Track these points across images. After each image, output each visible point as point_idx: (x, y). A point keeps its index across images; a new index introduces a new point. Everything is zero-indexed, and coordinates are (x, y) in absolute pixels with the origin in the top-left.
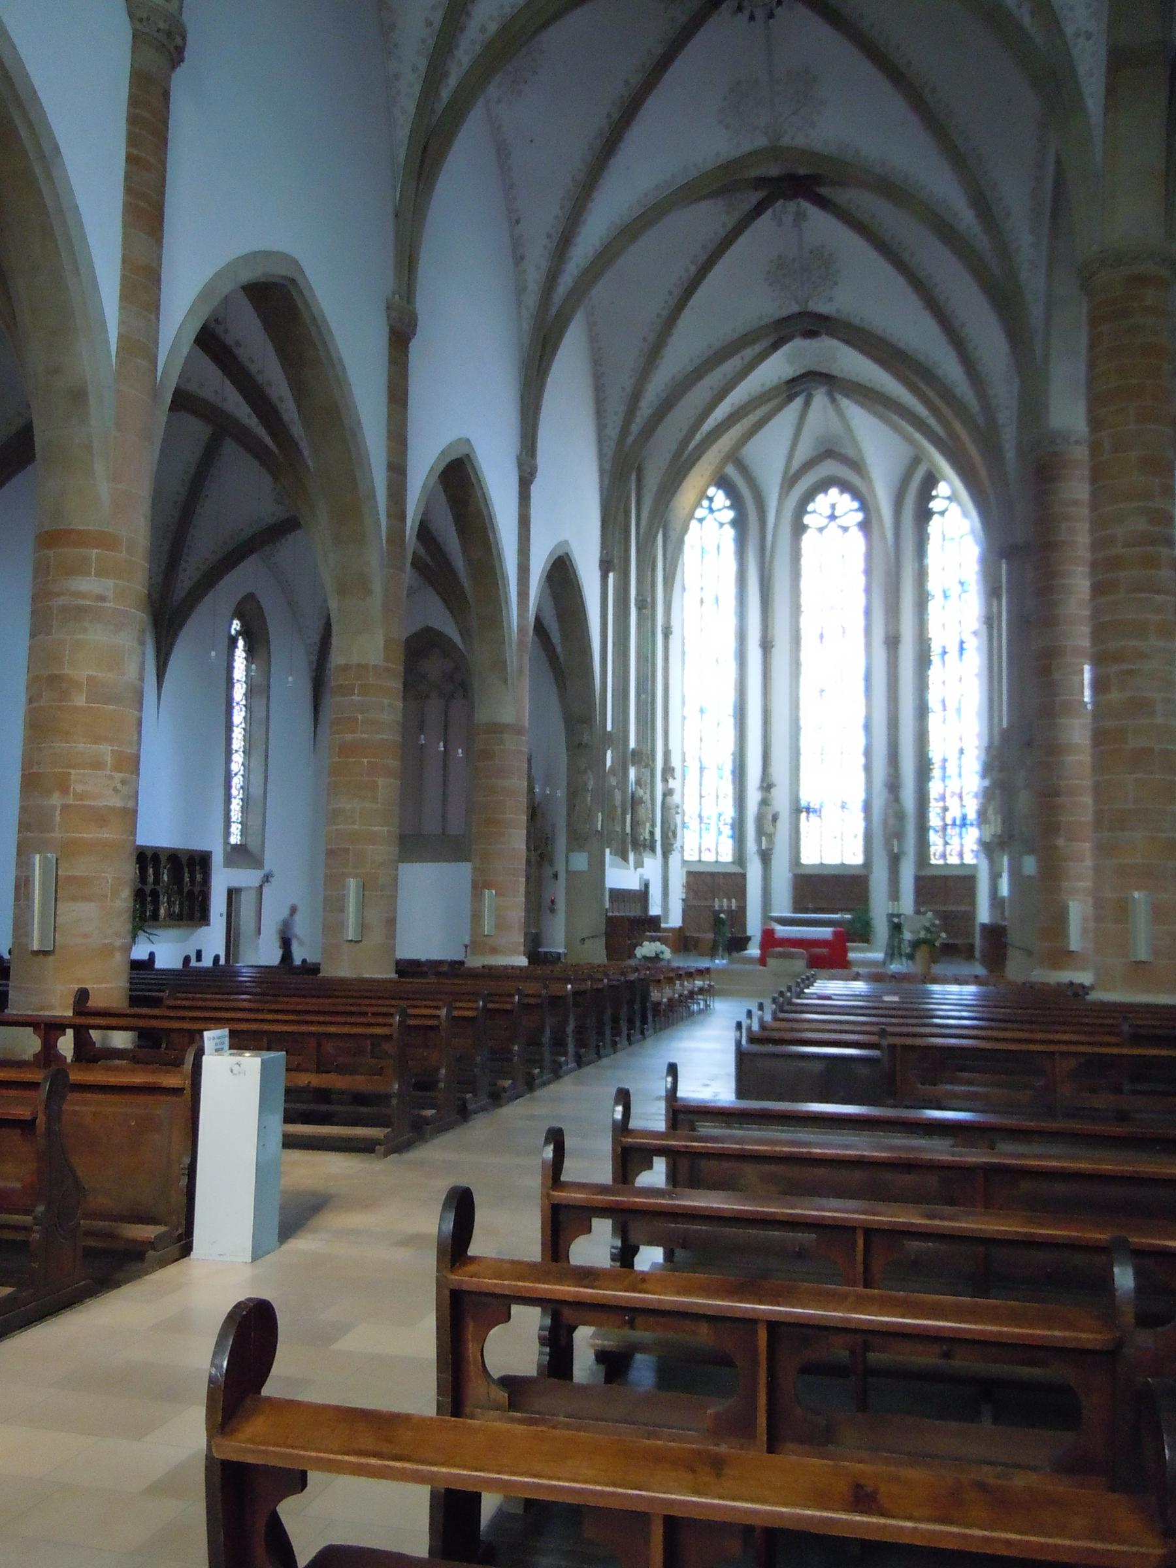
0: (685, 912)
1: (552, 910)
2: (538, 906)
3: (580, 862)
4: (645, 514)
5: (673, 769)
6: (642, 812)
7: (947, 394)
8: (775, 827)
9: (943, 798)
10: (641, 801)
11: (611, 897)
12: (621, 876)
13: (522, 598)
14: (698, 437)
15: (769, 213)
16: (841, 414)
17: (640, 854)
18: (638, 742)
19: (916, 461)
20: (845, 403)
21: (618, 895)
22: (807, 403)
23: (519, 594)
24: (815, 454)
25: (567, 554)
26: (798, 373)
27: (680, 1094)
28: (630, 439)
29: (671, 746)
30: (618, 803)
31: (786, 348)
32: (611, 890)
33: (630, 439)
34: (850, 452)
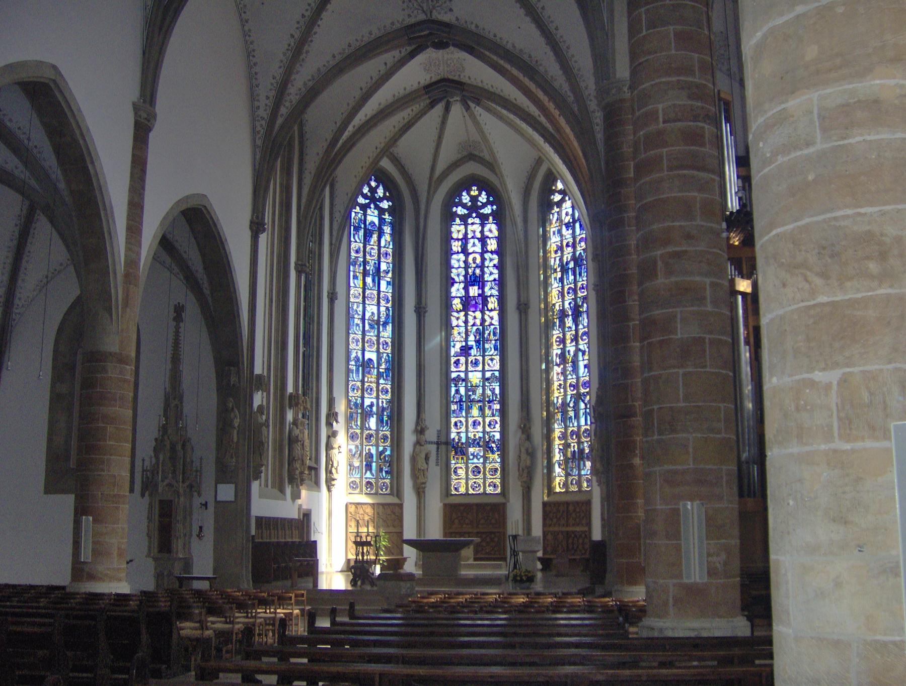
2: (165, 531)
5: (337, 414)
7: (546, 86)
13: (134, 234)
14: (350, 129)
15: (736, 472)
16: (473, 117)
17: (298, 487)
19: (539, 162)
20: (478, 110)
22: (447, 109)
23: (129, 229)
24: (460, 156)
26: (434, 80)
28: (280, 121)
31: (420, 58)
33: (280, 121)
34: (486, 156)
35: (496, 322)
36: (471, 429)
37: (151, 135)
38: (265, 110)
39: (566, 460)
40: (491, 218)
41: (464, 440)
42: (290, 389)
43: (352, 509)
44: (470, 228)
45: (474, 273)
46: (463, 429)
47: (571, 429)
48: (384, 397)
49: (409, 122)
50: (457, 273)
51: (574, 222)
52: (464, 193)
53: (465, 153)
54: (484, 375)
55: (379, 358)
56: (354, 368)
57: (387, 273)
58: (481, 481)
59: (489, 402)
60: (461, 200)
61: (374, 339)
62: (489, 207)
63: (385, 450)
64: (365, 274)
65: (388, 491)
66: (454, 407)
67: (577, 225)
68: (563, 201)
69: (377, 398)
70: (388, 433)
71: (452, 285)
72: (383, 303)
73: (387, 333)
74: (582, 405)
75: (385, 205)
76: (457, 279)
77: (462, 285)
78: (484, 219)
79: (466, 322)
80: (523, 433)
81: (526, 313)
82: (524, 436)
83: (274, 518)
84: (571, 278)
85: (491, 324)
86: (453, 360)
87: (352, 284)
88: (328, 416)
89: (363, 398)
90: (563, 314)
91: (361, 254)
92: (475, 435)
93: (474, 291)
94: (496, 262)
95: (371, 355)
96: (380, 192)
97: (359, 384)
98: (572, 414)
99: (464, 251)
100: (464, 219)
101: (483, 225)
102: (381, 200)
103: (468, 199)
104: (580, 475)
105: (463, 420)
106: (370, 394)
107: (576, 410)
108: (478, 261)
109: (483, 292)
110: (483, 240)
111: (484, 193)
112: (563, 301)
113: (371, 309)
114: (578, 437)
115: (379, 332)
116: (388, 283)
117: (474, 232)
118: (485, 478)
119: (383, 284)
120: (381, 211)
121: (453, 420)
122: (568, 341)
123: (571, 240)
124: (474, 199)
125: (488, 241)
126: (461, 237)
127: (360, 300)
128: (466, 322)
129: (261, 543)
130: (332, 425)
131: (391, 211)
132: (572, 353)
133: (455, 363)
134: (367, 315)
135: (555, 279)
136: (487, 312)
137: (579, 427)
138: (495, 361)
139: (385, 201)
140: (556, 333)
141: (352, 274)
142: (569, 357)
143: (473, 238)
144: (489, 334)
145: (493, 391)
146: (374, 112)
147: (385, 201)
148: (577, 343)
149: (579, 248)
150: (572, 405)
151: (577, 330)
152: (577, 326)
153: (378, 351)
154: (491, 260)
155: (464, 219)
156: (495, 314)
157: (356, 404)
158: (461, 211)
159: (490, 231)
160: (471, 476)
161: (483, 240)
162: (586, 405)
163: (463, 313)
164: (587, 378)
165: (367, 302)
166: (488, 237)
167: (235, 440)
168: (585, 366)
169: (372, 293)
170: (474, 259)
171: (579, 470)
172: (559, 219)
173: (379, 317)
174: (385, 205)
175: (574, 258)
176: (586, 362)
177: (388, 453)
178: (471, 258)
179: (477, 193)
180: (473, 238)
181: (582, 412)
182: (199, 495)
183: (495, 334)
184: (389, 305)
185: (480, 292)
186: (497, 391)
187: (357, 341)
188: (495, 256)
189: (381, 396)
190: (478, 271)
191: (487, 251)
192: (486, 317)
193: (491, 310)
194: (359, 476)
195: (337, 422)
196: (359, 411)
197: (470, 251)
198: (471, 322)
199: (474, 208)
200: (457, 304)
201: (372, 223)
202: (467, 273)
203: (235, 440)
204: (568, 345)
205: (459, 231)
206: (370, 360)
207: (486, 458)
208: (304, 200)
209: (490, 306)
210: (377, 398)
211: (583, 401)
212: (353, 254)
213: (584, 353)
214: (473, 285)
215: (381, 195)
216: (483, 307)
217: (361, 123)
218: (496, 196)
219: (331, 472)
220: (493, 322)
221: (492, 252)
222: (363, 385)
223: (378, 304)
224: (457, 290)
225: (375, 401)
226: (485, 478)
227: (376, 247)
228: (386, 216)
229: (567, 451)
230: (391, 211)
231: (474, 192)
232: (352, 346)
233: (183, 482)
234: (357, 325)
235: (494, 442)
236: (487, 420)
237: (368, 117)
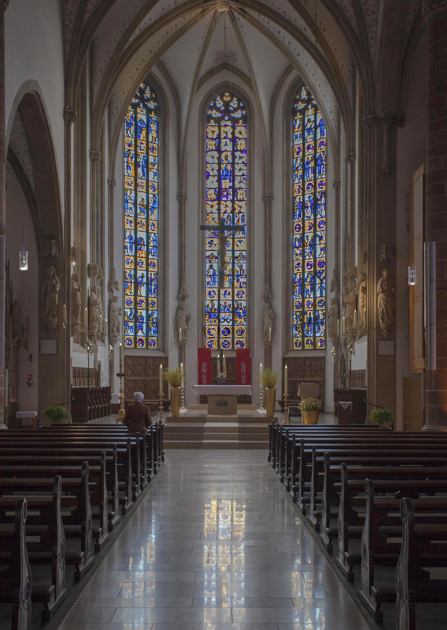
3: (50, 347)
10: (96, 303)
11: (74, 373)
12: (79, 358)
18: (92, 260)
21: (79, 372)
25: (37, 93)
28: (87, 16)
29: (115, 267)
30: (79, 302)
32: (75, 368)
33: (87, 16)
34: (241, 64)
35: (244, 210)
36: (222, 297)
37: (6, 14)
38: (74, 5)
39: (303, 325)
40: (241, 121)
41: (216, 307)
42: (88, 261)
43: (130, 362)
44: (223, 129)
45: (226, 169)
46: (216, 297)
47: (307, 300)
49: (181, 29)
50: (212, 168)
51: (316, 127)
53: (221, 62)
54: (233, 254)
55: (148, 238)
57: (154, 165)
58: (230, 340)
60: (215, 104)
61: (144, 221)
62: (239, 111)
63: (152, 314)
64: (137, 165)
67: (318, 130)
68: (306, 108)
69: (147, 270)
70: (155, 300)
71: (208, 177)
72: (151, 191)
74: (318, 281)
75: (152, 105)
76: (211, 173)
77: (216, 178)
78: (235, 121)
79: (219, 210)
81: (270, 204)
82: (267, 305)
84: (311, 175)
88: (110, 284)
89: (136, 270)
90: (303, 206)
91: (133, 148)
92: (225, 303)
94: (244, 160)
95: (142, 235)
96: (148, 94)
97: (132, 258)
98: (308, 287)
99: (218, 149)
100: (218, 121)
102: (148, 100)
103: (222, 103)
104: (315, 337)
106: (141, 267)
108: (230, 159)
109: (233, 184)
110: (234, 140)
111: (235, 99)
112: (303, 195)
113: (142, 195)
114: (314, 305)
115: (148, 215)
116: (155, 174)
117: (226, 133)
118: (233, 338)
119: (151, 174)
120: (149, 111)
121: (208, 290)
124: (226, 104)
125: (239, 142)
126: (215, 136)
127: (132, 187)
128: (219, 210)
129: (76, 388)
131: (157, 110)
132: (310, 239)
134: (139, 200)
136: (237, 202)
137: (315, 298)
138: (242, 243)
142: (308, 241)
144: (238, 221)
145: (241, 267)
147: (152, 102)
148: (315, 231)
149: (318, 151)
150: (308, 280)
151: (315, 220)
152: (315, 216)
153: (147, 232)
154: (241, 158)
155: (218, 121)
158: (215, 114)
159: (240, 133)
161: (234, 140)
162: (322, 281)
163: (217, 202)
165: (138, 190)
166: (238, 138)
167: (57, 302)
168: (322, 249)
170: (226, 157)
171: (315, 333)
173: (148, 203)
175: (315, 159)
176: (323, 246)
177: (155, 316)
179: (229, 99)
181: (317, 286)
182: (26, 348)
184: (156, 193)
185: (231, 184)
186: (244, 267)
187: (131, 222)
189: (150, 269)
190: (229, 167)
191: (237, 150)
192: (236, 206)
193: (240, 201)
195: (117, 289)
197: (223, 149)
198: (223, 209)
199: (227, 111)
201: (141, 121)
202: (220, 168)
203: (57, 302)
204: (306, 231)
205: (213, 132)
206: (141, 239)
207: (233, 321)
208: (95, 96)
209: (239, 197)
210: (147, 270)
211: (319, 277)
212: (127, 147)
214: (225, 179)
215: (149, 96)
216: (233, 198)
217: (146, 26)
220: (242, 210)
225: (145, 273)
226: (233, 338)
227: (144, 142)
228: (153, 115)
229: (303, 317)
230: (157, 110)
233: (13, 337)
234: (131, 208)
235: (241, 309)
236: (236, 291)
237: (153, 21)
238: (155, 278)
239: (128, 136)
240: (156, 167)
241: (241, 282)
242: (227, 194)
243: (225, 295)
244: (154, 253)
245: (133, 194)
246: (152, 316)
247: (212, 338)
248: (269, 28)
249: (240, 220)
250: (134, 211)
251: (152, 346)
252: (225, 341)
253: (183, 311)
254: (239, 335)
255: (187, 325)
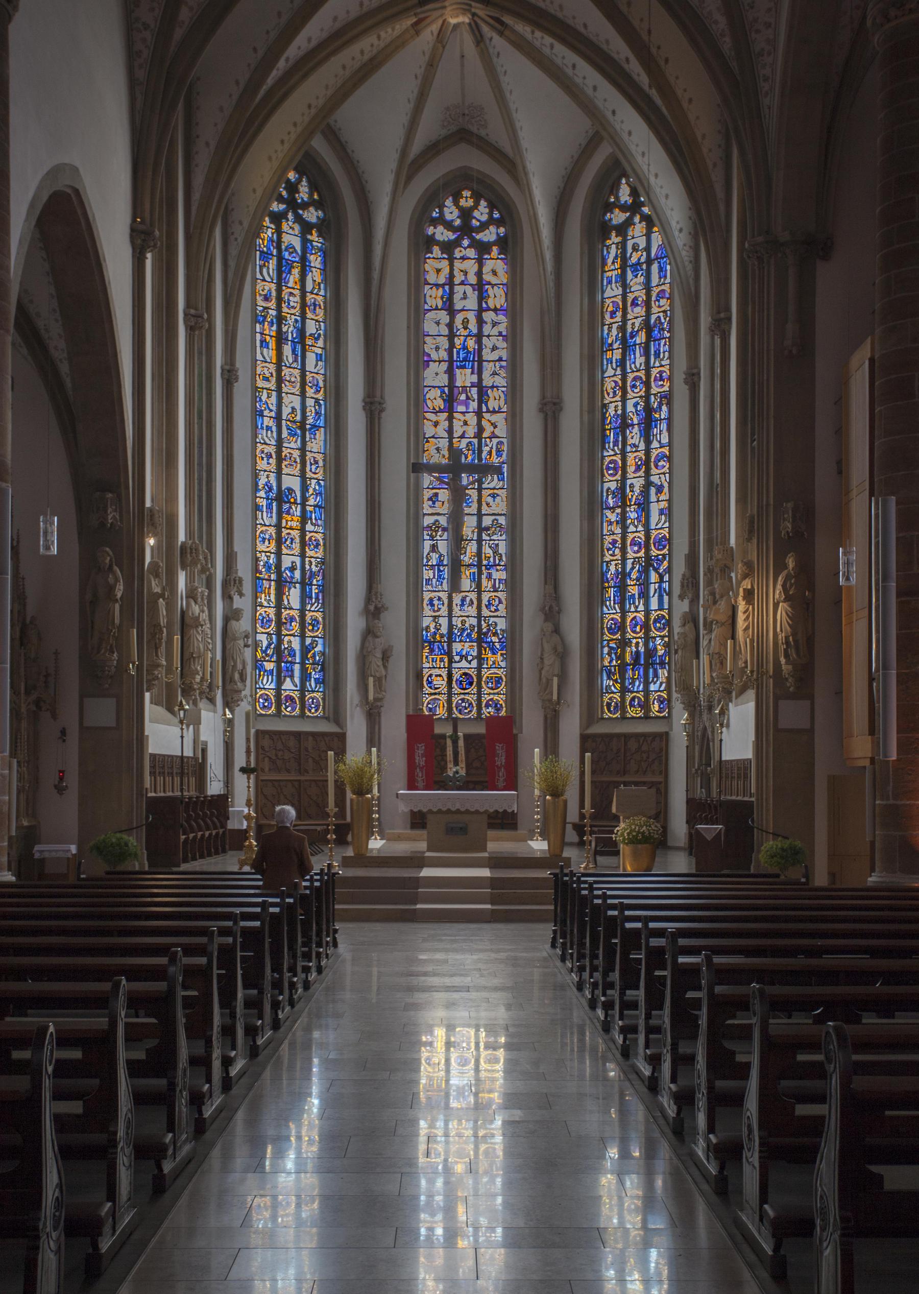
0: (19, 1061)
1: (60, 789)
3: (103, 712)
4: (199, 180)
6: (198, 639)
8: (385, 667)
9: (621, 627)
10: (197, 623)
11: (153, 767)
12: (163, 736)
18: (190, 533)
24: (444, 132)
27: (724, 758)
28: (178, 34)
30: (163, 621)
32: (153, 756)
33: (178, 34)
34: (496, 133)
35: (501, 431)
36: (456, 610)
37: (12, 28)
39: (623, 668)
40: (495, 249)
41: (444, 630)
44: (458, 265)
45: (465, 347)
46: (444, 611)
48: (312, 553)
49: (371, 60)
50: (436, 346)
51: (649, 262)
52: (449, 202)
53: (454, 128)
54: (480, 521)
55: (304, 488)
56: (265, 503)
57: (317, 339)
58: (472, 698)
59: (488, 567)
61: (296, 454)
62: (492, 229)
63: (314, 644)
64: (280, 339)
65: (320, 713)
66: (428, 574)
67: (655, 268)
68: (629, 223)
69: (303, 555)
71: (427, 364)
72: (310, 392)
73: (317, 444)
74: (654, 577)
75: (312, 215)
76: (434, 356)
77: (444, 366)
78: (483, 248)
79: (450, 431)
80: (546, 620)
82: (549, 626)
83: (169, 756)
84: (640, 360)
85: (493, 436)
86: (427, 494)
87: (259, 357)
88: (226, 584)
89: (279, 554)
90: (624, 424)
91: (272, 304)
92: (463, 623)
93: (465, 377)
94: (502, 328)
95: (292, 482)
96: (304, 193)
97: (272, 531)
98: (634, 590)
99: (449, 307)
100: (448, 248)
101: (480, 262)
102: (305, 206)
103: (456, 212)
104: (647, 692)
105: (444, 596)
107: (644, 585)
108: (473, 327)
109: (480, 379)
110: (481, 287)
111: (483, 203)
112: (624, 400)
113: (292, 401)
114: (646, 626)
115: (304, 443)
116: (319, 358)
119: (311, 358)
120: (306, 228)
121: (427, 596)
122: (631, 469)
123: (642, 295)
124: (466, 214)
126: (442, 280)
127: (272, 385)
128: (450, 431)
130: (231, 598)
132: (637, 490)
133: (430, 499)
134: (286, 411)
135: (610, 361)
137: (647, 612)
138: (498, 499)
139: (312, 209)
140: (611, 454)
141: (258, 336)
142: (634, 495)
143: (462, 283)
144: (490, 453)
146: (325, 35)
147: (312, 209)
149: (655, 309)
150: (634, 575)
151: (648, 452)
152: (648, 443)
154: (495, 324)
155: (448, 248)
156: (499, 418)
157: (267, 566)
158: (442, 234)
159: (494, 273)
160: (456, 689)
161: (481, 287)
162: (661, 577)
164: (665, 532)
167: (117, 621)
168: (661, 512)
169: (291, 373)
170: (465, 323)
171: (647, 684)
172: (624, 258)
173: (304, 417)
174: (312, 215)
176: (664, 505)
177: (319, 648)
178: (459, 318)
179: (471, 202)
180: (462, 283)
181: (652, 588)
182: (54, 716)
183: (499, 453)
184: (320, 396)
185: (475, 378)
186: (502, 549)
187: (269, 456)
188: (501, 318)
189: (309, 553)
190: (471, 344)
191: (488, 309)
192: (484, 423)
193: (494, 412)
194: (273, 686)
195: (241, 595)
196: (273, 577)
198: (458, 430)
200: (434, 399)
201: (291, 248)
202: (452, 345)
203: (117, 621)
204: (630, 475)
205: (438, 271)
206: (290, 490)
207: (480, 659)
208: (196, 196)
209: (492, 404)
210: (303, 555)
211: (656, 570)
212: (260, 302)
213: (660, 489)
214: (463, 367)
216: (480, 407)
218: (506, 213)
219: (232, 680)
220: (497, 432)
221: (495, 310)
222: (279, 533)
223: (303, 394)
224: (435, 376)
225: (298, 560)
227: (297, 292)
228: (314, 236)
229: (623, 652)
230: (322, 227)
231: (466, 202)
232: (262, 465)
234: (269, 428)
235: (495, 634)
237: (314, 43)
238: (319, 571)
239: (264, 280)
240: (320, 343)
241: (495, 580)
242: (468, 398)
243: (462, 605)
244: (316, 519)
245: (273, 399)
246: (313, 648)
247: (435, 694)
248: (554, 57)
249: (494, 452)
250: (275, 434)
251: (313, 711)
252: (463, 700)
253: (377, 640)
254: (492, 689)
255: (385, 667)
